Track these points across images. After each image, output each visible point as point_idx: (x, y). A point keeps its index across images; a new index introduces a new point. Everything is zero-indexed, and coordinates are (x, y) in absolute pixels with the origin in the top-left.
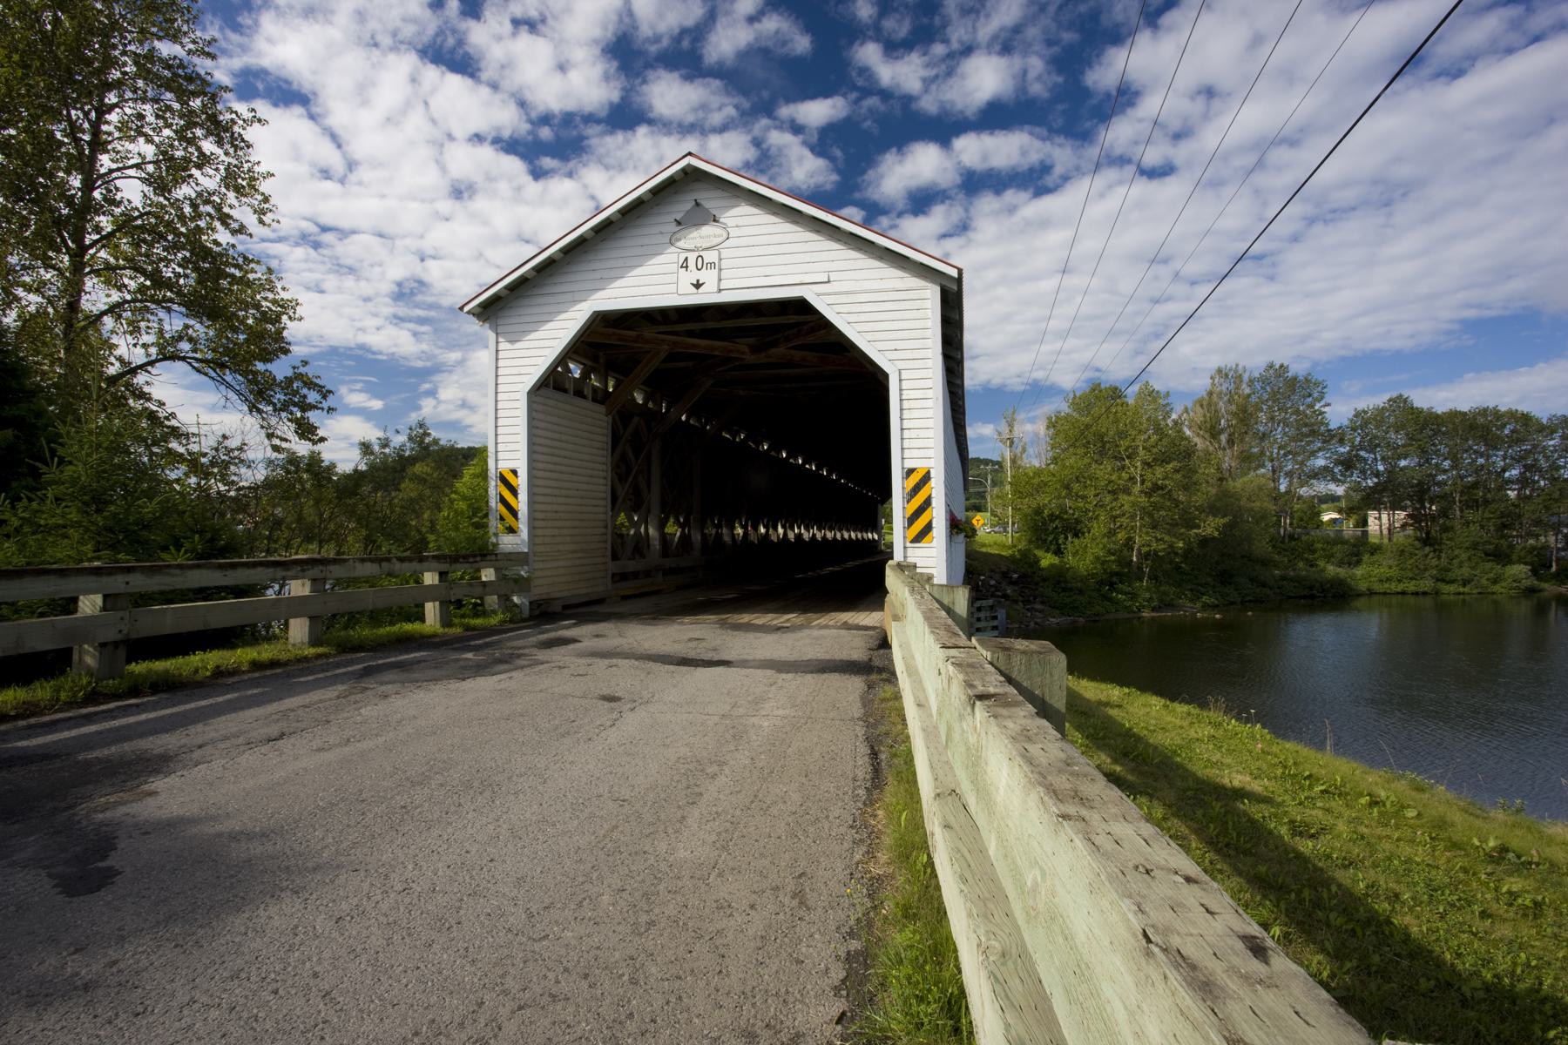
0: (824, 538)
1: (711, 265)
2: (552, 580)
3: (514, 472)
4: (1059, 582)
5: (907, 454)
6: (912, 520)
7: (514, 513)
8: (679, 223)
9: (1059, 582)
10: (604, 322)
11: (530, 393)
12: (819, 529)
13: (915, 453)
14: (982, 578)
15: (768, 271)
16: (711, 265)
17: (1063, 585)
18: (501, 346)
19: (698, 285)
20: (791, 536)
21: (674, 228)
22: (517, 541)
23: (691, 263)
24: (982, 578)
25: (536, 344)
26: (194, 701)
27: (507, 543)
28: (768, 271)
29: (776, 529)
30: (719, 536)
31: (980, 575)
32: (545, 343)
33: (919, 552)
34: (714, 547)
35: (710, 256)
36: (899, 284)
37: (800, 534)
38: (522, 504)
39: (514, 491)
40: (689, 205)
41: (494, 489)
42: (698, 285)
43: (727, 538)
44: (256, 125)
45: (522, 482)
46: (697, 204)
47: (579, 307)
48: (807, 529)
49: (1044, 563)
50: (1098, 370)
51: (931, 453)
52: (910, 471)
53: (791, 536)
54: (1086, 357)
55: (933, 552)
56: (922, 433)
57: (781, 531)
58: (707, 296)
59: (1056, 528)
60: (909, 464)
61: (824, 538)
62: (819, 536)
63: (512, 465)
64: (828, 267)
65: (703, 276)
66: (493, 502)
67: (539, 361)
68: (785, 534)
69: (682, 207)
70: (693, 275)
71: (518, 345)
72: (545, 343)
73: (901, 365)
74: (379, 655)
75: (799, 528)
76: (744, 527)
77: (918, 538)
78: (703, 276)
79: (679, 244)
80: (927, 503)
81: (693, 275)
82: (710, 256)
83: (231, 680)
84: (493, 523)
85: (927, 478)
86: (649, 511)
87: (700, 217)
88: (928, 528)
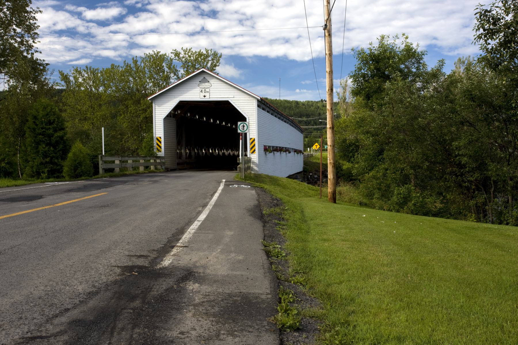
0: (234, 154)
1: (208, 92)
2: (168, 165)
3: (160, 138)
4: (349, 177)
5: (250, 135)
6: (251, 149)
7: (160, 147)
8: (200, 82)
9: (349, 177)
10: (182, 105)
11: (164, 119)
12: (232, 151)
13: (252, 135)
14: (311, 174)
15: (220, 94)
16: (208, 92)
17: (351, 178)
18: (156, 107)
19: (205, 96)
20: (221, 153)
21: (199, 83)
22: (162, 154)
23: (203, 91)
24: (311, 174)
25: (166, 107)
26: (11, 214)
27: (160, 154)
28: (220, 94)
29: (215, 151)
30: (198, 153)
31: (310, 173)
32: (168, 107)
33: (253, 155)
34: (198, 156)
35: (207, 90)
36: (249, 99)
37: (224, 153)
38: (162, 145)
39: (160, 142)
40: (202, 78)
41: (155, 142)
42: (205, 96)
43: (201, 153)
44: (39, 13)
45: (162, 140)
46: (204, 78)
47: (176, 99)
48: (227, 150)
49: (345, 167)
50: (435, 38)
51: (255, 135)
52: (251, 139)
53: (221, 153)
54: (428, 29)
55: (256, 155)
56: (253, 131)
57: (217, 151)
58: (207, 99)
59: (353, 149)
60: (251, 137)
61: (234, 154)
62: (231, 154)
63: (160, 136)
64: (234, 94)
65: (207, 94)
66: (155, 145)
67: (167, 111)
68: (219, 153)
69: (201, 78)
70: (204, 94)
71: (160, 107)
72: (168, 107)
73: (249, 116)
74: (86, 193)
75: (224, 150)
76: (198, 150)
77: (253, 153)
78: (207, 94)
79: (201, 86)
80: (254, 145)
81: (204, 94)
82: (207, 90)
83: (141, 175)
84: (155, 150)
85: (254, 140)
86: (182, 146)
87: (205, 81)
88: (255, 150)
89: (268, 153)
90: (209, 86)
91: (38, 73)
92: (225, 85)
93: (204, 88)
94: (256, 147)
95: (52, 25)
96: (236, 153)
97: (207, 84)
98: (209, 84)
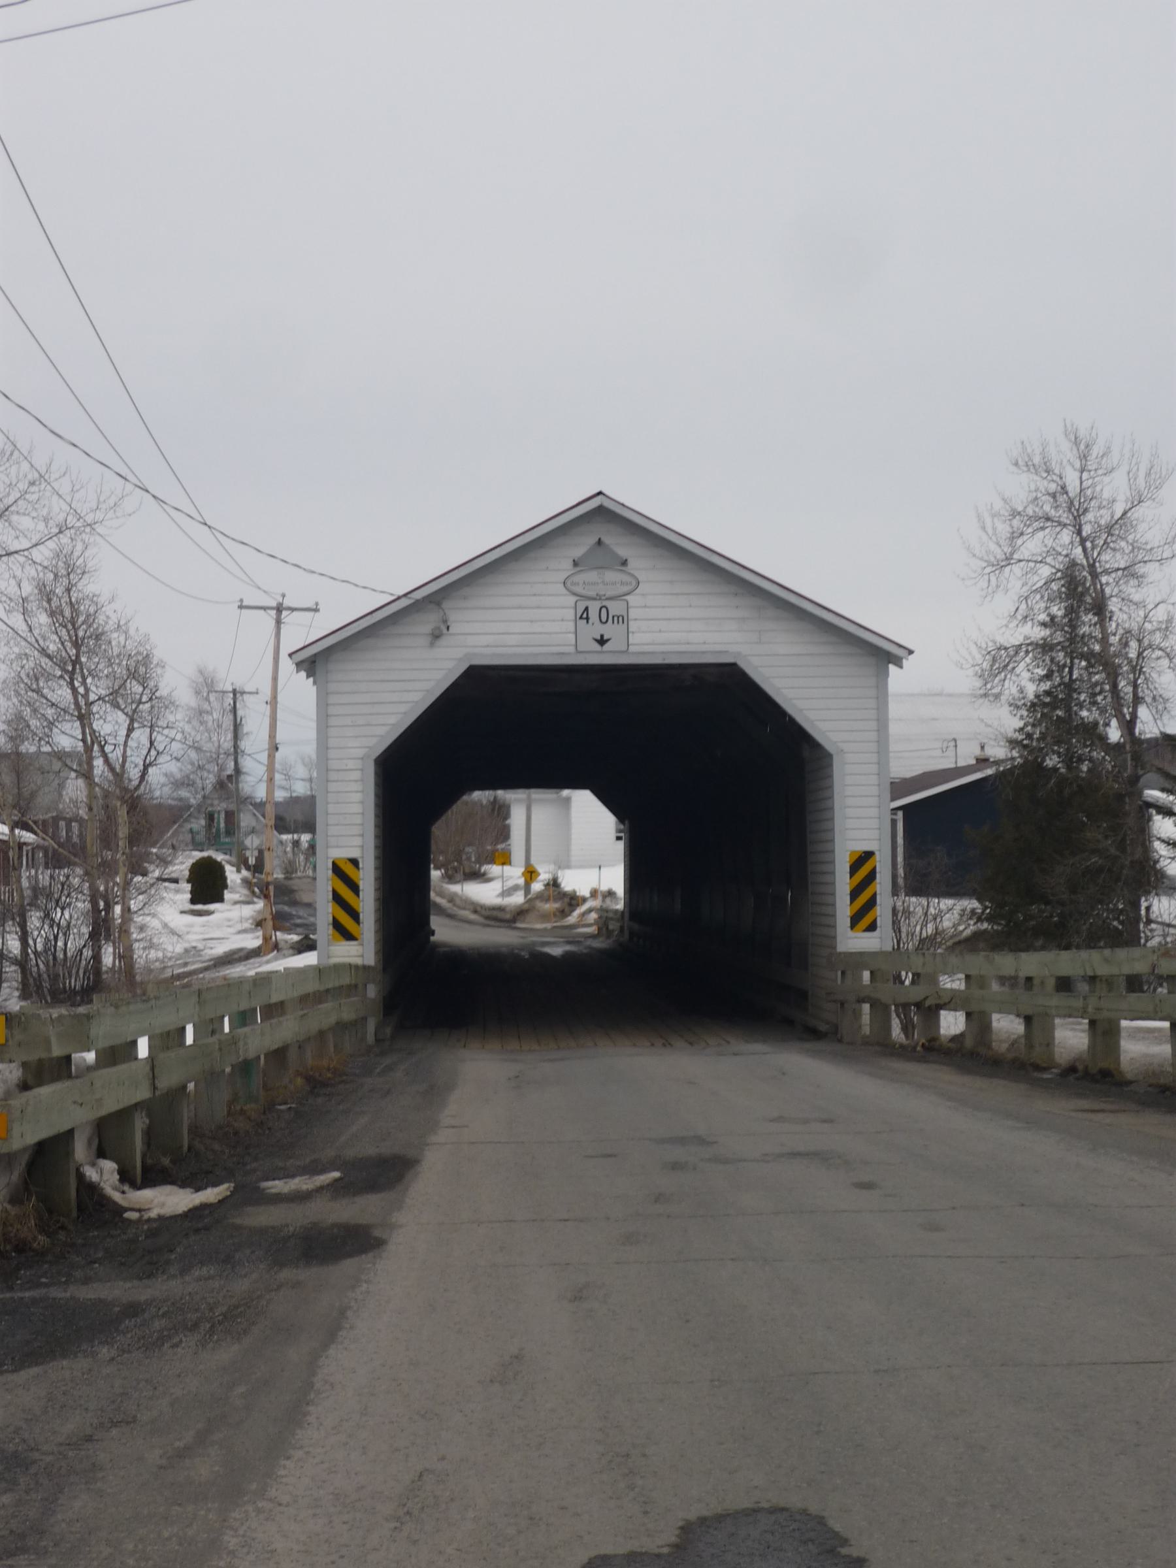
7: (355, 915)
19: (602, 641)
39: (354, 888)
42: (602, 641)
45: (367, 879)
46: (599, 542)
63: (354, 853)
65: (608, 630)
80: (855, 894)
81: (597, 630)
89: (1013, 974)
90: (626, 589)
91: (951, 1002)
92: (96, 19)
93: (598, 598)
94: (843, 883)
95: (1051, 983)
96: (51, 821)
97: (611, 576)
98: (626, 578)
